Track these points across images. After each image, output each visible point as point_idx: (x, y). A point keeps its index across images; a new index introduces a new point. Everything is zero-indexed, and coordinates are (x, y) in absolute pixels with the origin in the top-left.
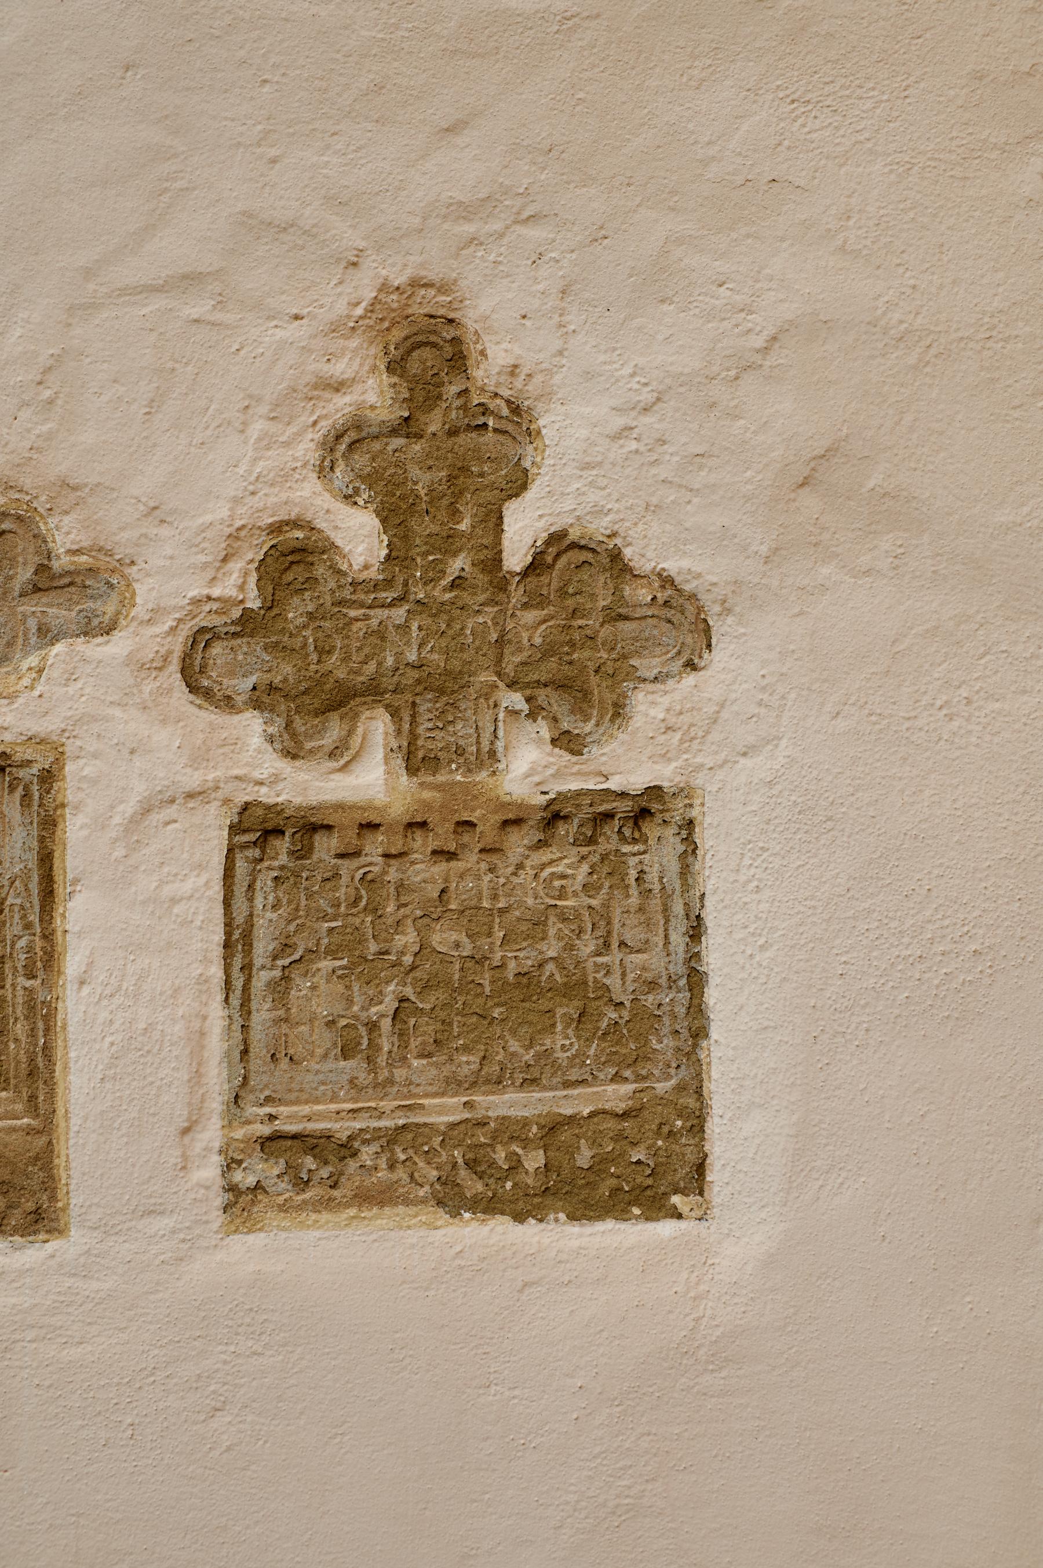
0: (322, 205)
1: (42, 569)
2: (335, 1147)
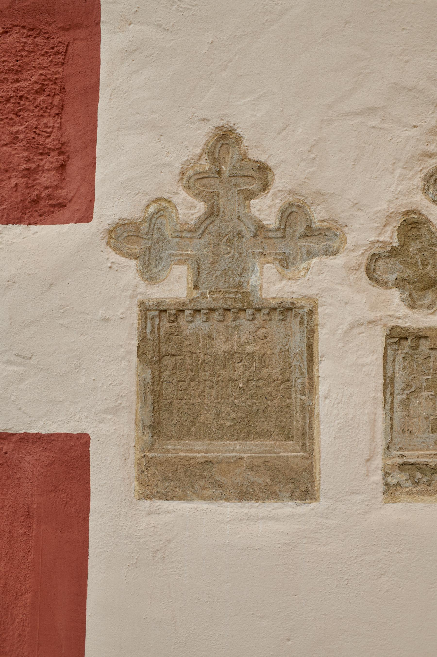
0: (427, 80)
1: (308, 227)
2: (430, 469)
